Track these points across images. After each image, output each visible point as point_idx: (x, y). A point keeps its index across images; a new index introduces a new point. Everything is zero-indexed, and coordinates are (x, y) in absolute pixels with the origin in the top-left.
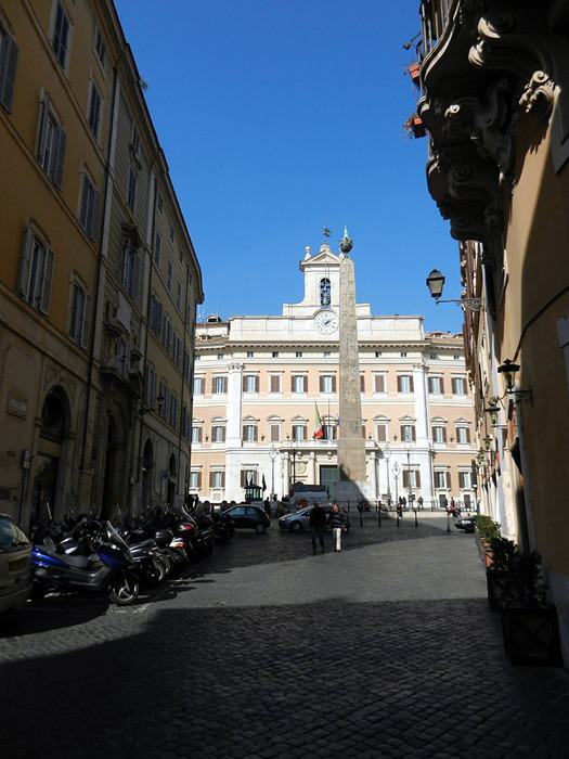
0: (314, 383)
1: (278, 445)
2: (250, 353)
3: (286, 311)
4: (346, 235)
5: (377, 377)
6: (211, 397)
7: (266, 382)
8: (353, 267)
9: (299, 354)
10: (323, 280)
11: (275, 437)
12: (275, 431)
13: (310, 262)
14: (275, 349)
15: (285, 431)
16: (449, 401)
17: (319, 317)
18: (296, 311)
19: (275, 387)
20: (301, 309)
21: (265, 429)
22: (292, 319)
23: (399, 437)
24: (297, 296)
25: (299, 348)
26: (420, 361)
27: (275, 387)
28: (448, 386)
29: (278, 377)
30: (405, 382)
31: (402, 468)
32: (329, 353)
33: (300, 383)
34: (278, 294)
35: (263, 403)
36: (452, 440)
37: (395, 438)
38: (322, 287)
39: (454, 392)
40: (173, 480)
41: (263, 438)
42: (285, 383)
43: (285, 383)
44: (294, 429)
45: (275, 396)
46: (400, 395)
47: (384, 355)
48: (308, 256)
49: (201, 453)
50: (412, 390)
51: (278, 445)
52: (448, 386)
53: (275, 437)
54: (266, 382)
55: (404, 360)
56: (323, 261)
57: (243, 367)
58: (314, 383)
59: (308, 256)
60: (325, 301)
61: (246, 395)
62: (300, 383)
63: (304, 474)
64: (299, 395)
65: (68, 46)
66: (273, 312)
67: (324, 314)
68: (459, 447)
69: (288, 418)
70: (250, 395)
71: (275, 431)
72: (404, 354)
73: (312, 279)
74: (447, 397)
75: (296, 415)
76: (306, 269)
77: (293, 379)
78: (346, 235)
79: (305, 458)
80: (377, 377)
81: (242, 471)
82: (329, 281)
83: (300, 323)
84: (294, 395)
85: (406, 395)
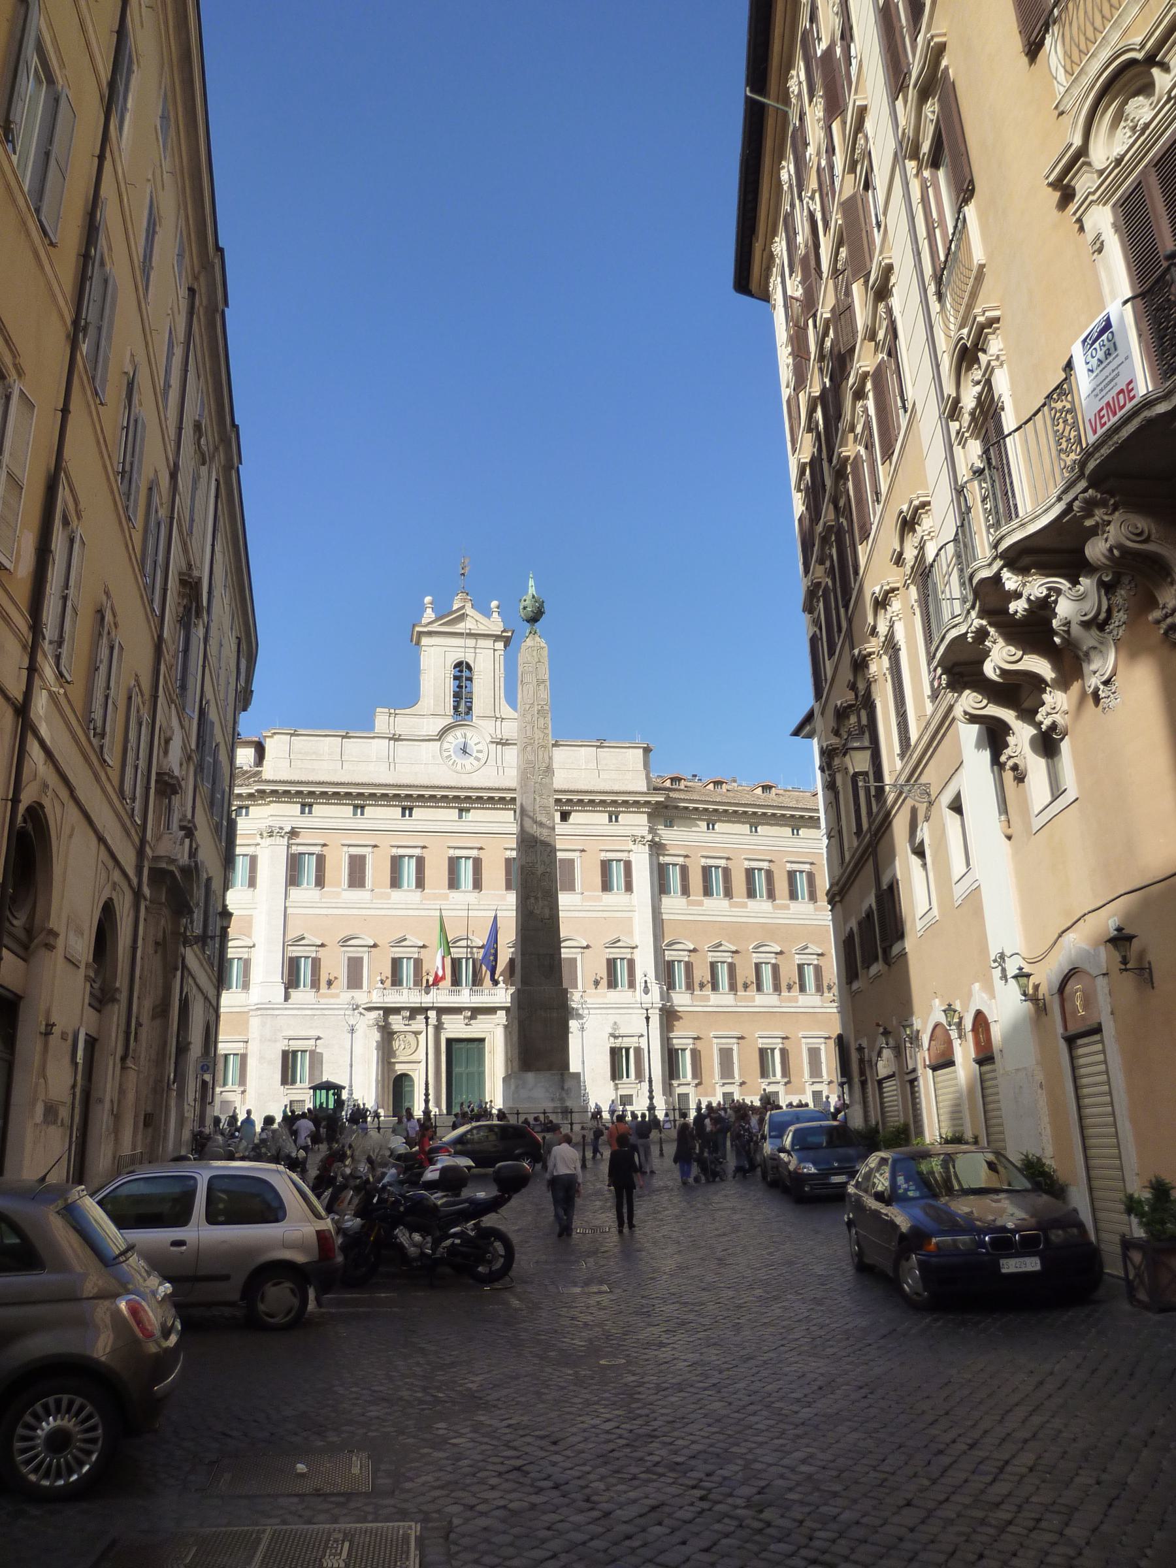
0: (437, 871)
1: (361, 997)
2: (306, 807)
3: (382, 720)
4: (532, 591)
5: (352, 857)
6: (787, 907)
7: (338, 868)
8: (545, 652)
9: (407, 810)
10: (458, 665)
11: (354, 982)
12: (355, 966)
13: (435, 627)
14: (359, 798)
15: (376, 968)
16: (781, 913)
17: (450, 738)
18: (404, 723)
19: (357, 877)
20: (415, 720)
21: (335, 964)
22: (395, 738)
23: (604, 982)
24: (406, 695)
25: (408, 800)
26: (644, 831)
27: (357, 877)
28: (781, 885)
29: (572, 861)
30: (618, 872)
31: (283, 1045)
32: (468, 810)
33: (409, 870)
34: (374, 685)
35: (328, 908)
36: (790, 988)
37: (597, 983)
38: (456, 678)
39: (793, 896)
40: (207, 1077)
41: (330, 983)
42: (377, 870)
43: (377, 870)
44: (396, 963)
45: (357, 895)
46: (607, 898)
47: (473, 815)
48: (429, 615)
49: (504, 1021)
50: (629, 887)
51: (361, 997)
52: (781, 885)
53: (354, 982)
54: (338, 868)
55: (613, 829)
56: (460, 627)
57: (293, 833)
58: (437, 871)
59: (429, 615)
60: (462, 708)
61: (294, 892)
62: (409, 870)
63: (413, 1058)
64: (407, 896)
65: (129, 105)
66: (354, 722)
67: (459, 732)
68: (760, 999)
69: (332, 940)
70: (305, 893)
71: (355, 966)
72: (613, 817)
73: (436, 660)
74: (737, 905)
75: (399, 935)
76: (425, 641)
77: (453, 863)
78: (532, 591)
79: (419, 1023)
80: (352, 857)
81: (285, 1054)
82: (469, 667)
83: (407, 748)
84: (396, 895)
85: (617, 898)
